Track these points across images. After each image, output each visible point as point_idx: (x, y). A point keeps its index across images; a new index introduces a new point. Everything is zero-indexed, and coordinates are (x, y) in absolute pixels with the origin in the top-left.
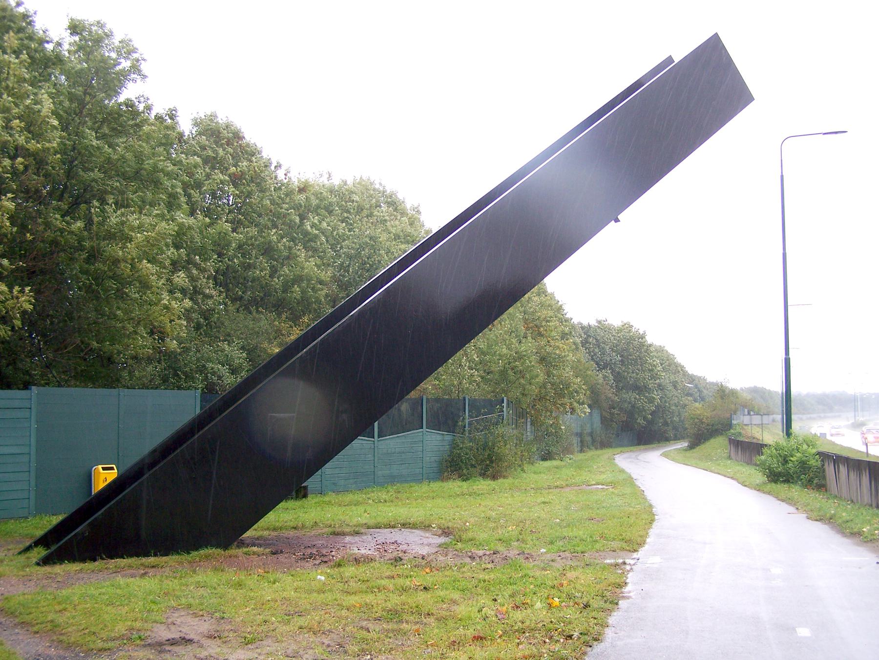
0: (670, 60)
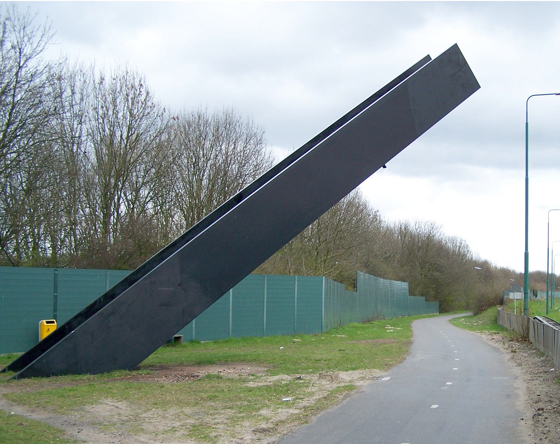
0: (428, 57)
